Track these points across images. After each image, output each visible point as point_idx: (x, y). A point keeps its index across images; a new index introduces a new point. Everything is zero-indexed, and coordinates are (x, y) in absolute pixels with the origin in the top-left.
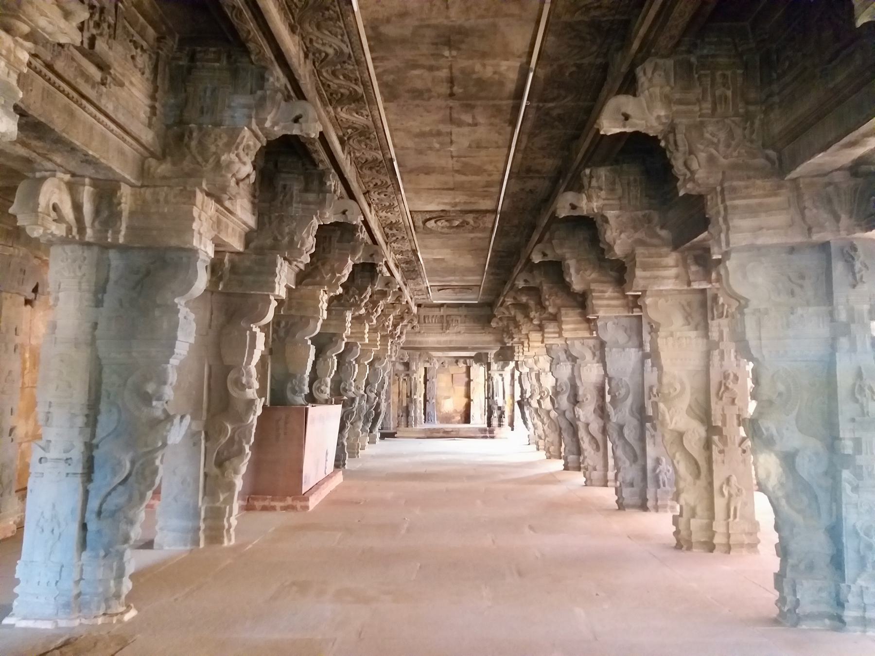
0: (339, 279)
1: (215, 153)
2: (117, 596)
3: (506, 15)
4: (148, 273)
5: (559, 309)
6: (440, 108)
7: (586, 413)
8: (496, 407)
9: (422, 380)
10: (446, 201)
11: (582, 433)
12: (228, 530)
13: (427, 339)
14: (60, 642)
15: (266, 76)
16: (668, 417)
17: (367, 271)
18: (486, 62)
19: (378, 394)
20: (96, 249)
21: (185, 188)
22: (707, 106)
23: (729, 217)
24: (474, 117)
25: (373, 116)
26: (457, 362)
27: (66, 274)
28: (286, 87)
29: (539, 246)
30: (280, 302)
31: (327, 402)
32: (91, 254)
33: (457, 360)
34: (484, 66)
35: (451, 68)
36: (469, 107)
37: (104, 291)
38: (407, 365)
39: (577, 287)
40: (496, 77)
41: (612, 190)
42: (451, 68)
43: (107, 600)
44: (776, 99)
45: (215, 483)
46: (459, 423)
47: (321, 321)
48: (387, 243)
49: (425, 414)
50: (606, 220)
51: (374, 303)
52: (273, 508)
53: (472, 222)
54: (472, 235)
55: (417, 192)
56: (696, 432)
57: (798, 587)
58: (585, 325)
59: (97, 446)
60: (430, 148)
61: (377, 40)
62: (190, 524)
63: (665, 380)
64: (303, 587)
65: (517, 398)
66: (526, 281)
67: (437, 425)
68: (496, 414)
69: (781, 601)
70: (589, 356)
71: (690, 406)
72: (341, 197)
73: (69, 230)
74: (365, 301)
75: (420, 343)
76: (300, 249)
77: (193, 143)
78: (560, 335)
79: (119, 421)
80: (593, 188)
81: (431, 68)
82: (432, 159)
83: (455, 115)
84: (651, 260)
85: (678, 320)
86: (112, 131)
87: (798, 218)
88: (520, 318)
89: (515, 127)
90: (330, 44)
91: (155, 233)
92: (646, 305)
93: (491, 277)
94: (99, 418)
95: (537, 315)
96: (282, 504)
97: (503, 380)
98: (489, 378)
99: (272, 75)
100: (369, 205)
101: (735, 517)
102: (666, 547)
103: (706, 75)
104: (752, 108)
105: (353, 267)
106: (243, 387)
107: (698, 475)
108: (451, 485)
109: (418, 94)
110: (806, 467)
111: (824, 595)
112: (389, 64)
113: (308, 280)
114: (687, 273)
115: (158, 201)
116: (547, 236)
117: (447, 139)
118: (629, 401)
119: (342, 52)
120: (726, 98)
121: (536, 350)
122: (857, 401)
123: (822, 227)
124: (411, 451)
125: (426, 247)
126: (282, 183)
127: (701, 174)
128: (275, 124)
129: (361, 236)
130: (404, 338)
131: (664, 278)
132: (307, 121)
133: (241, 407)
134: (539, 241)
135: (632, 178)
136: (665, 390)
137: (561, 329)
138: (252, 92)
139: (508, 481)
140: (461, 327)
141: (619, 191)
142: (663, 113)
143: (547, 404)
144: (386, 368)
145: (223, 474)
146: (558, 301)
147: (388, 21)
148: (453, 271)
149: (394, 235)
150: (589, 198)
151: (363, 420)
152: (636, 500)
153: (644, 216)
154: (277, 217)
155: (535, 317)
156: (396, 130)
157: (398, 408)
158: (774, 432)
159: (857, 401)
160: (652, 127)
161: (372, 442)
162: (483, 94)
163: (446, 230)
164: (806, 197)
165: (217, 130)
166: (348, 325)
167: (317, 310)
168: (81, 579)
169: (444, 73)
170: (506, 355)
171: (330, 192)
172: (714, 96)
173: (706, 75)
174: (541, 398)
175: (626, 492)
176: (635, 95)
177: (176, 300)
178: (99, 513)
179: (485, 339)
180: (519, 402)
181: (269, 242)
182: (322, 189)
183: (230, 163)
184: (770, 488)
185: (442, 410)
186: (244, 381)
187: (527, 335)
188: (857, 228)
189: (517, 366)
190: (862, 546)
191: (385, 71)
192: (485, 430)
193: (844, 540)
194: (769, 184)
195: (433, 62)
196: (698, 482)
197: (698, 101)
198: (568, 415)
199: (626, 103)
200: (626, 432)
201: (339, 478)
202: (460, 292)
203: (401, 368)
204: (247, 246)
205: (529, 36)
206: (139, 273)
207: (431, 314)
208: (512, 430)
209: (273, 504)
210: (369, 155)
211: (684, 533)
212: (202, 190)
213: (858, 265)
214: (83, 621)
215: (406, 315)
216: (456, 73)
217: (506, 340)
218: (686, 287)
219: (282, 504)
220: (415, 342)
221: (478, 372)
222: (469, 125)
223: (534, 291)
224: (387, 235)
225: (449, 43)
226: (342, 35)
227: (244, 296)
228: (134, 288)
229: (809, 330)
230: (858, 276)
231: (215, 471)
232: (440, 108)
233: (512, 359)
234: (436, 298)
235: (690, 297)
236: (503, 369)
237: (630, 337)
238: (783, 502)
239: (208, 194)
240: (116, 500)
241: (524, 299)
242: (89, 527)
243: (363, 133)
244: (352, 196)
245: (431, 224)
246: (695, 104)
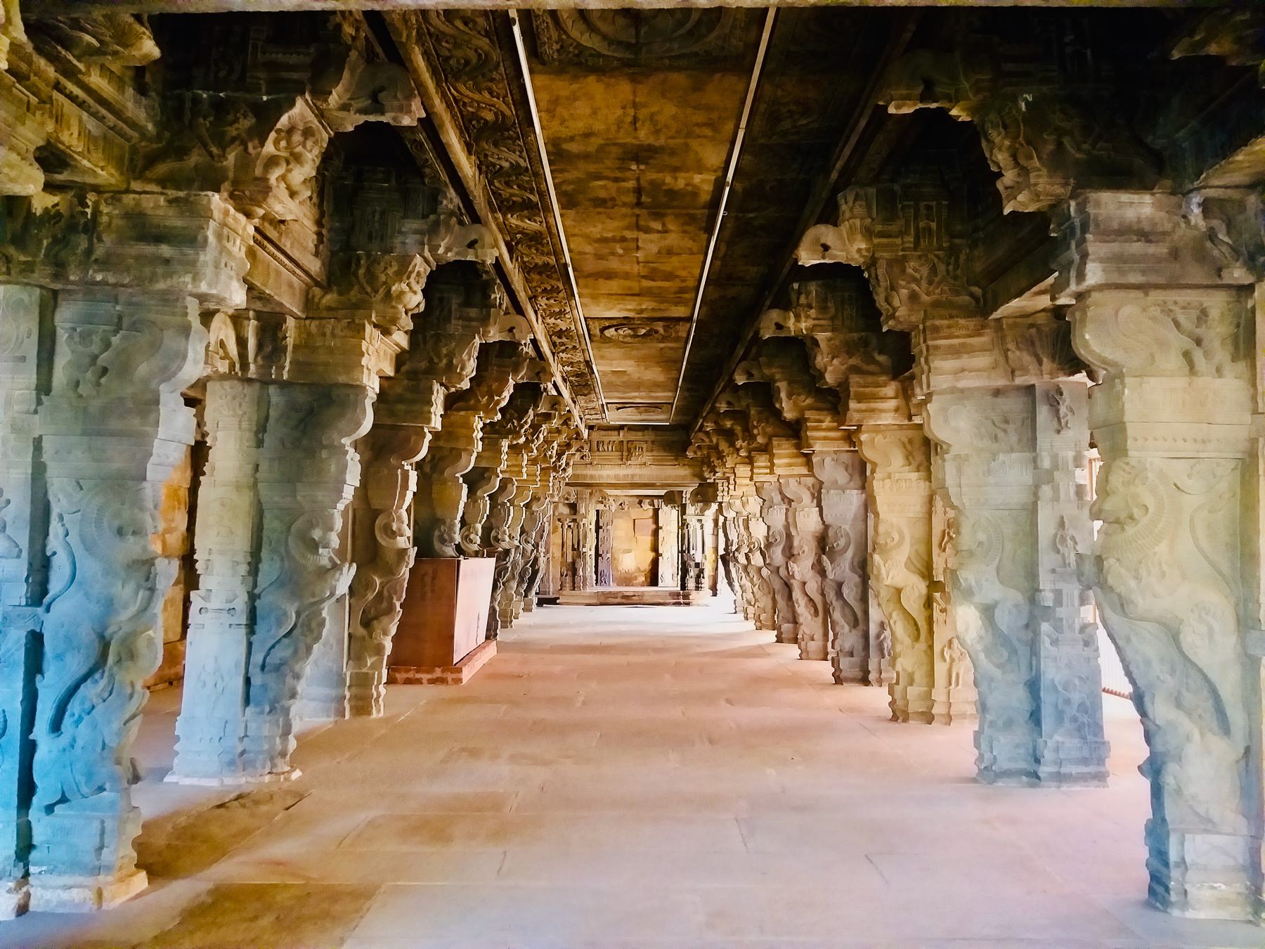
0: (498, 402)
1: (385, 283)
2: (283, 754)
3: (699, 137)
4: (311, 412)
5: (770, 439)
6: (625, 216)
7: (802, 569)
8: (692, 564)
9: (593, 527)
10: (629, 307)
11: (797, 594)
12: (377, 700)
13: (601, 473)
14: (233, 796)
15: (440, 198)
16: (883, 571)
17: (529, 393)
18: (677, 174)
19: (536, 546)
20: (257, 385)
21: (353, 321)
22: (910, 239)
23: (930, 358)
24: (664, 225)
25: (547, 223)
26: (640, 503)
27: (225, 413)
28: (459, 209)
29: (743, 364)
30: (436, 435)
31: (477, 554)
32: (251, 391)
33: (641, 500)
34: (676, 179)
35: (638, 179)
36: (658, 216)
37: (265, 430)
38: (573, 507)
39: (789, 415)
40: (689, 188)
41: (823, 309)
42: (638, 179)
43: (272, 759)
44: (981, 235)
45: (359, 647)
46: (643, 586)
47: (475, 455)
48: (553, 354)
49: (596, 573)
50: (816, 343)
51: (535, 428)
52: (419, 682)
53: (661, 331)
54: (662, 345)
55: (595, 298)
56: (915, 588)
57: (995, 743)
58: (801, 460)
59: (259, 596)
60: (613, 254)
61: (558, 155)
62: (333, 693)
63: (881, 529)
64: (474, 753)
65: (721, 552)
66: (729, 403)
67: (613, 588)
68: (693, 572)
69: (981, 758)
70: (807, 498)
71: (909, 558)
72: (507, 313)
73: (232, 366)
74: (526, 427)
75: (592, 477)
76: (460, 374)
77: (361, 271)
78: (772, 472)
79: (282, 568)
80: (801, 305)
81: (616, 180)
82: (614, 264)
83: (642, 223)
84: (867, 390)
85: (897, 459)
86: (285, 266)
87: (1002, 360)
88: (723, 446)
89: (711, 234)
90: (506, 158)
91: (321, 369)
92: (861, 442)
93: (687, 394)
94: (260, 566)
95: (745, 444)
96: (429, 676)
97: (702, 527)
98: (683, 524)
99: (446, 197)
100: (536, 312)
101: (957, 684)
102: (880, 719)
103: (909, 206)
104: (957, 241)
105: (521, 394)
106: (393, 535)
107: (917, 638)
108: (632, 658)
109: (600, 203)
110: (1004, 619)
111: (1022, 751)
112: (572, 175)
113: (460, 404)
114: (908, 405)
115: (324, 335)
116: (754, 351)
117: (633, 245)
118: (850, 554)
119: (518, 165)
120: (930, 229)
121: (744, 489)
122: (1058, 552)
123: (1025, 371)
124: (575, 620)
125: (602, 357)
126: (438, 295)
127: (902, 312)
128: (448, 249)
129: (525, 350)
130: (570, 471)
131: (882, 411)
132: (483, 247)
133: (391, 557)
134: (744, 358)
135: (846, 295)
136: (881, 540)
137: (773, 464)
138: (425, 217)
139: (705, 654)
140: (647, 457)
141: (832, 311)
142: (863, 246)
143: (757, 559)
144: (546, 510)
145: (371, 637)
146: (769, 430)
147: (572, 139)
148: (638, 386)
149: (563, 344)
150: (798, 318)
151: (519, 580)
152: (857, 673)
153: (860, 339)
154: (432, 336)
155: (741, 447)
156: (574, 235)
157: (562, 563)
158: (973, 584)
159: (1058, 552)
160: (852, 259)
161: (527, 609)
162: (675, 203)
163: (628, 340)
164: (1009, 339)
165: (387, 257)
166: (504, 457)
167: (471, 441)
168: (246, 736)
169: (631, 184)
170: (706, 494)
171: (495, 306)
172: (917, 229)
173: (909, 206)
174: (751, 550)
175: (845, 663)
176: (836, 225)
177: (343, 441)
178: (263, 667)
179: (677, 474)
180: (723, 557)
181: (423, 365)
182: (487, 304)
183: (402, 293)
184: (969, 642)
185: (620, 568)
186: (394, 528)
187: (733, 468)
188: (1061, 373)
189: (720, 511)
190: (1060, 701)
191: (564, 182)
192: (678, 594)
193: (1042, 694)
194: (971, 323)
195: (618, 174)
196: (917, 645)
197: (901, 234)
198: (783, 572)
199: (826, 233)
200: (845, 591)
201: (492, 650)
202: (646, 411)
203: (565, 510)
204: (397, 370)
205: (724, 156)
206: (301, 408)
207: (606, 439)
208: (715, 594)
209: (418, 676)
210: (540, 260)
211: (899, 703)
212: (371, 322)
213: (1063, 410)
214: (249, 779)
215: (573, 442)
216: (644, 183)
217: (706, 475)
218: (906, 422)
219: (429, 676)
220: (585, 476)
221: (669, 516)
222: (658, 232)
223: (741, 416)
224: (554, 344)
225: (637, 159)
226: (521, 152)
227: (394, 428)
228: (296, 427)
229: (1012, 476)
230: (1063, 421)
231: (361, 631)
232: (625, 216)
233: (714, 500)
234: (613, 417)
235: (910, 433)
236: (702, 512)
237: (851, 476)
238: (982, 656)
239: (375, 326)
240: (281, 653)
241: (728, 424)
242: (252, 682)
243: (535, 239)
244: (520, 311)
245: (610, 333)
246: (897, 237)
